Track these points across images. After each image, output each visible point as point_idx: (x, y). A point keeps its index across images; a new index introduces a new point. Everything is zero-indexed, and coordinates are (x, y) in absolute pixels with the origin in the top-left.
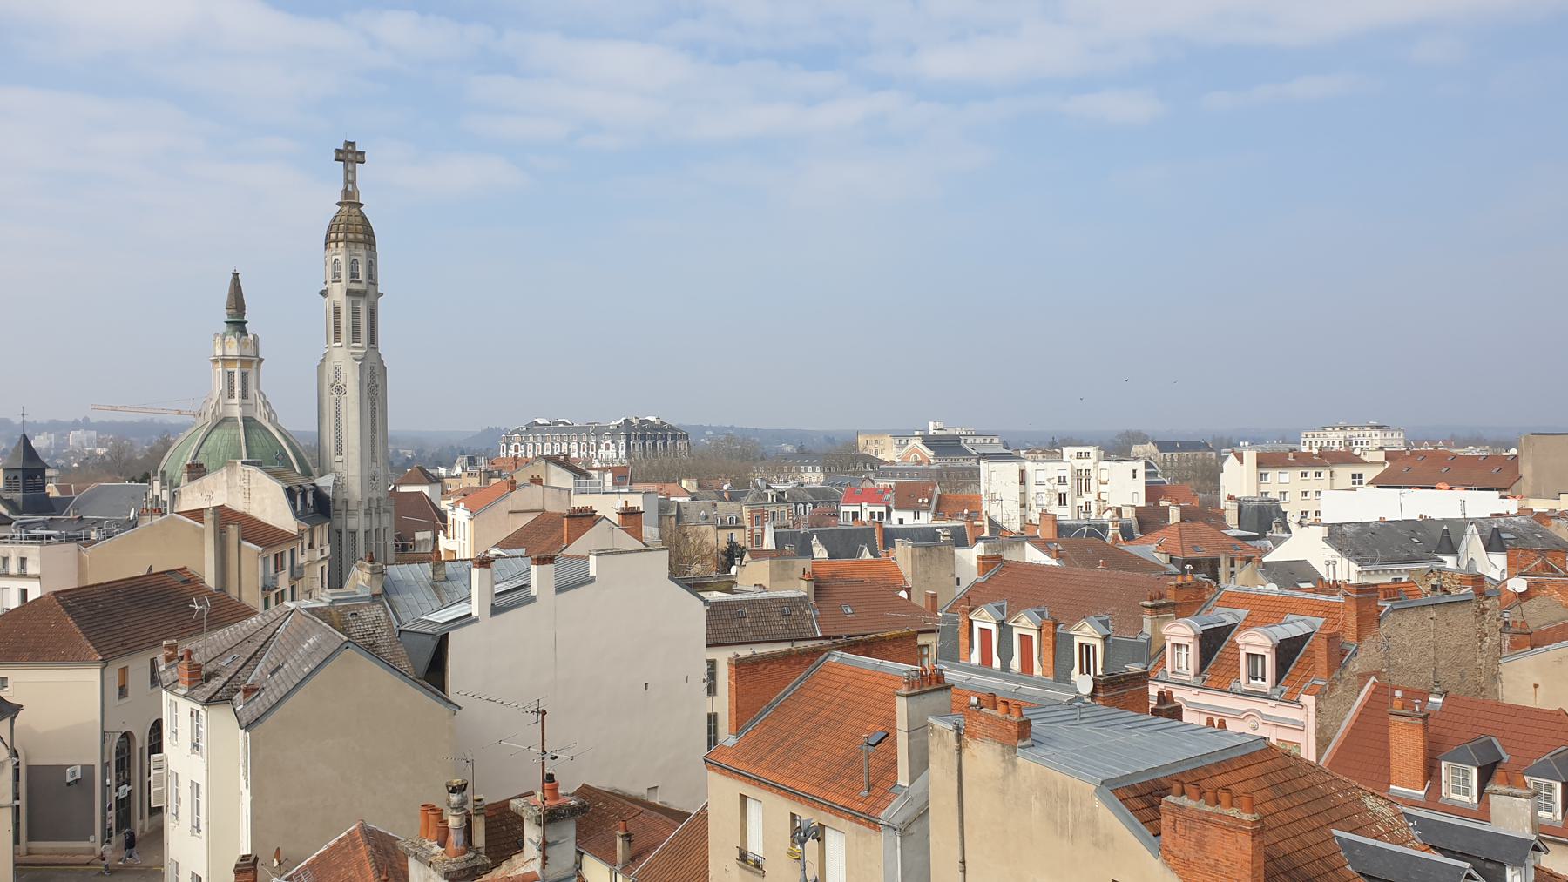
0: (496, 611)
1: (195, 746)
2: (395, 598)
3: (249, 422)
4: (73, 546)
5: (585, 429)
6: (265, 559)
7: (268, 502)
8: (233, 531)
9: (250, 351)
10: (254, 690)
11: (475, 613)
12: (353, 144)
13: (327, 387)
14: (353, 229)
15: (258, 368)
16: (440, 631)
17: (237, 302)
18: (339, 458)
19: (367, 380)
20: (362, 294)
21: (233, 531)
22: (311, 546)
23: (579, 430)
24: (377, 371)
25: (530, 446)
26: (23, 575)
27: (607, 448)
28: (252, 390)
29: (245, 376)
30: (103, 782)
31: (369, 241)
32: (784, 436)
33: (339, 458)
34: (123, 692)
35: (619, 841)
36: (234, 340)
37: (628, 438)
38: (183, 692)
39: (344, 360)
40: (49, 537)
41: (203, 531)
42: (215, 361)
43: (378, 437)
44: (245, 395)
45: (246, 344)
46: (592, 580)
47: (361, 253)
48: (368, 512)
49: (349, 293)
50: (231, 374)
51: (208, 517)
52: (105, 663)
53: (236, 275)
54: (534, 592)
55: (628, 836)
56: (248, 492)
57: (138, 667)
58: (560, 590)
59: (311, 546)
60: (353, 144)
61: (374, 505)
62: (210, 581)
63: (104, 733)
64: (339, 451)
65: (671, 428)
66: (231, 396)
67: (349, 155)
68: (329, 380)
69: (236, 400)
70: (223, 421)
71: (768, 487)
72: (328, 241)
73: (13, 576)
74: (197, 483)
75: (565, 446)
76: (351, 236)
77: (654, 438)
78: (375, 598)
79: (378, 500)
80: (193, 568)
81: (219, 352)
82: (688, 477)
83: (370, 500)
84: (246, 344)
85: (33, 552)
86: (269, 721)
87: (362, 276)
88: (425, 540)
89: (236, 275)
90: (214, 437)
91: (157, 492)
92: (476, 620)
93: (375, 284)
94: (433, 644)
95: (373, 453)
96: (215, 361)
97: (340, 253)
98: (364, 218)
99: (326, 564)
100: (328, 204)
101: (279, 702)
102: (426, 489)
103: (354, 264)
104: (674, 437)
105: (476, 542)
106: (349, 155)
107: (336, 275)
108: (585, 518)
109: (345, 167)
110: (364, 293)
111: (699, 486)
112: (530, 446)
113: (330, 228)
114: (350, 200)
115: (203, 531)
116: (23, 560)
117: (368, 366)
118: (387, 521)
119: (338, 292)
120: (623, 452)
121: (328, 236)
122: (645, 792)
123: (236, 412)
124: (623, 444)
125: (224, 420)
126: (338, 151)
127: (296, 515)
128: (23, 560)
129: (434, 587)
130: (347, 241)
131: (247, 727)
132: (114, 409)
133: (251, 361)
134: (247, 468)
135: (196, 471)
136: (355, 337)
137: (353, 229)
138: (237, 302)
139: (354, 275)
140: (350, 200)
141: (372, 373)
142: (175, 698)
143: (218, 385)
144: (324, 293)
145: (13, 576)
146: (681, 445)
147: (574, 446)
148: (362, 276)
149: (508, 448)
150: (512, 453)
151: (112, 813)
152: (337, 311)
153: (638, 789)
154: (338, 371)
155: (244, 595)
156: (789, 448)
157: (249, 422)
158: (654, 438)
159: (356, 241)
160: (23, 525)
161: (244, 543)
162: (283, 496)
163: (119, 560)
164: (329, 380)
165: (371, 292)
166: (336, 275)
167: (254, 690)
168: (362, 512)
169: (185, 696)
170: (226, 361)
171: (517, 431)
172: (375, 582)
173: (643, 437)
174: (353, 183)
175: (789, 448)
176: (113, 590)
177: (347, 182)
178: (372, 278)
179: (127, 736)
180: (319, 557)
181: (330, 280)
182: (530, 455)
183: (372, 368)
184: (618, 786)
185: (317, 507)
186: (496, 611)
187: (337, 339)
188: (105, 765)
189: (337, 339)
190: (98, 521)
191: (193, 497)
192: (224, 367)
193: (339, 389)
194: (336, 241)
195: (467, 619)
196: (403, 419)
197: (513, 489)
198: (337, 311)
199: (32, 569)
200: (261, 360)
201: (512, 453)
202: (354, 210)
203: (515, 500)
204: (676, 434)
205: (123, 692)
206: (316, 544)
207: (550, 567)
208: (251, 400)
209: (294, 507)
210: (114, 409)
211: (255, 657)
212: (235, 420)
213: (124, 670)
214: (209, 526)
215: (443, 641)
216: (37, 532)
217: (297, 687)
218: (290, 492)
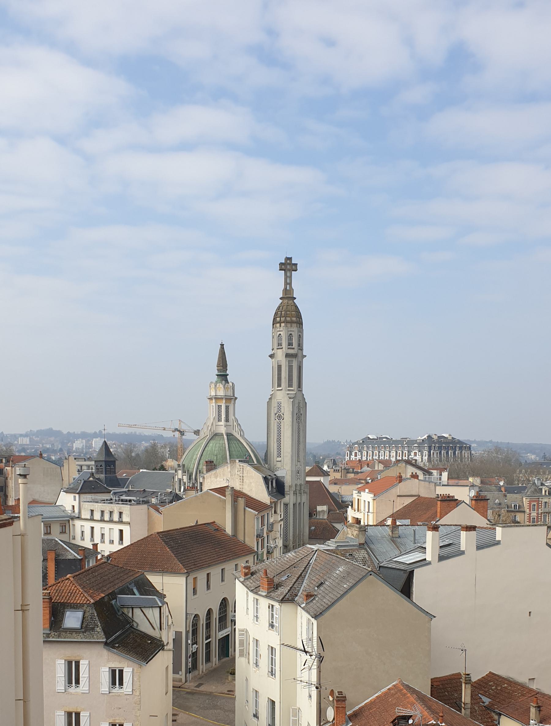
0: (441, 558)
1: (272, 626)
2: (372, 546)
3: (229, 435)
4: (145, 506)
5: (401, 442)
6: (258, 518)
7: (255, 487)
8: (241, 502)
9: (230, 393)
10: (311, 596)
11: (429, 559)
12: (290, 259)
13: (273, 414)
14: (289, 315)
15: (234, 404)
16: (409, 568)
17: (223, 363)
18: (279, 459)
19: (296, 411)
20: (295, 356)
21: (241, 502)
22: (275, 512)
23: (396, 442)
24: (301, 405)
25: (365, 453)
26: (121, 522)
27: (415, 454)
28: (231, 417)
29: (227, 408)
30: (187, 642)
31: (300, 323)
32: (530, 448)
33: (279, 459)
34: (195, 592)
35: (533, 710)
36: (221, 386)
37: (430, 448)
38: (264, 594)
39: (282, 397)
40: (130, 501)
41: (225, 500)
42: (211, 399)
43: (301, 446)
44: (227, 420)
45: (228, 388)
46: (498, 543)
47: (294, 329)
48: (295, 493)
49: (287, 355)
50: (219, 407)
51: (228, 492)
52: (188, 574)
53: (222, 345)
54: (463, 548)
55: (539, 707)
56: (242, 479)
57: (201, 576)
58: (479, 548)
59: (275, 512)
60: (290, 259)
61: (298, 488)
62: (229, 530)
63: (187, 614)
64: (279, 455)
65: (459, 442)
66: (220, 420)
67: (288, 266)
68: (274, 410)
69: (223, 423)
70: (216, 435)
71: (542, 484)
72: (274, 322)
73: (116, 522)
74: (213, 472)
75: (387, 453)
76: (288, 319)
77: (447, 449)
78: (361, 546)
79: (301, 485)
80: (219, 522)
81: (213, 394)
82: (473, 476)
83: (296, 485)
84: (228, 388)
85: (126, 509)
86: (327, 614)
87: (295, 345)
88: (323, 511)
89: (222, 345)
90: (211, 445)
91: (180, 477)
92: (430, 563)
93: (302, 350)
94: (405, 576)
95: (298, 456)
96: (211, 399)
97: (283, 331)
98: (296, 307)
99: (282, 523)
100: (274, 300)
101: (333, 604)
102: (321, 479)
103: (290, 336)
104: (461, 448)
105: (377, 513)
106: (288, 266)
107: (280, 344)
108: (450, 502)
109: (286, 274)
110: (295, 356)
111: (482, 482)
112: (365, 453)
113: (276, 314)
114: (288, 295)
115: (225, 500)
116: (121, 513)
117: (297, 402)
118: (305, 498)
119: (280, 355)
120: (426, 458)
121: (274, 319)
122: (527, 681)
123: (222, 430)
124: (426, 453)
125: (216, 435)
126: (281, 264)
127: (270, 493)
128: (121, 513)
129: (393, 541)
130: (286, 322)
131: (316, 617)
132: (130, 426)
133: (231, 399)
134: (242, 464)
135: (211, 466)
136: (290, 385)
137: (289, 315)
138: (223, 363)
139: (290, 344)
140: (288, 295)
141: (299, 407)
142: (257, 597)
143: (212, 413)
144: (272, 356)
145: (116, 522)
146: (466, 453)
147: (393, 453)
148: (295, 345)
149: (351, 454)
150: (353, 457)
151: (190, 660)
152: (279, 367)
153: (522, 679)
154: (279, 404)
155: (247, 539)
156: (533, 457)
157: (229, 435)
158: (447, 449)
159: (292, 322)
160: (115, 493)
161: (247, 509)
162: (262, 481)
163: (183, 516)
164: (274, 410)
165: (300, 355)
166: (280, 344)
167: (311, 596)
168: (292, 493)
169: (266, 597)
170: (217, 398)
171: (356, 443)
172: (361, 536)
173: (440, 448)
174: (290, 284)
175: (533, 457)
176: (183, 532)
177: (286, 283)
178: (300, 346)
179: (196, 616)
180: (279, 519)
181: (276, 347)
182: (393, 459)
183: (299, 403)
184: (511, 676)
185: (277, 487)
186: (441, 558)
187: (279, 385)
188: (187, 632)
189: (279, 385)
190: (154, 492)
191: (212, 481)
192: (216, 402)
193: (280, 417)
194: (280, 322)
195: (423, 562)
196: (315, 437)
197: (400, 481)
198: (279, 367)
199: (125, 518)
200: (236, 398)
201: (359, 457)
202: (291, 302)
203: (401, 488)
204: (463, 446)
205: (195, 592)
206: (278, 512)
207: (474, 533)
208: (230, 423)
209: (268, 488)
210: (130, 426)
211: (301, 577)
212: (222, 435)
213: (195, 579)
214: (228, 498)
215: (411, 573)
216: (124, 497)
217: (342, 596)
218: (266, 479)
